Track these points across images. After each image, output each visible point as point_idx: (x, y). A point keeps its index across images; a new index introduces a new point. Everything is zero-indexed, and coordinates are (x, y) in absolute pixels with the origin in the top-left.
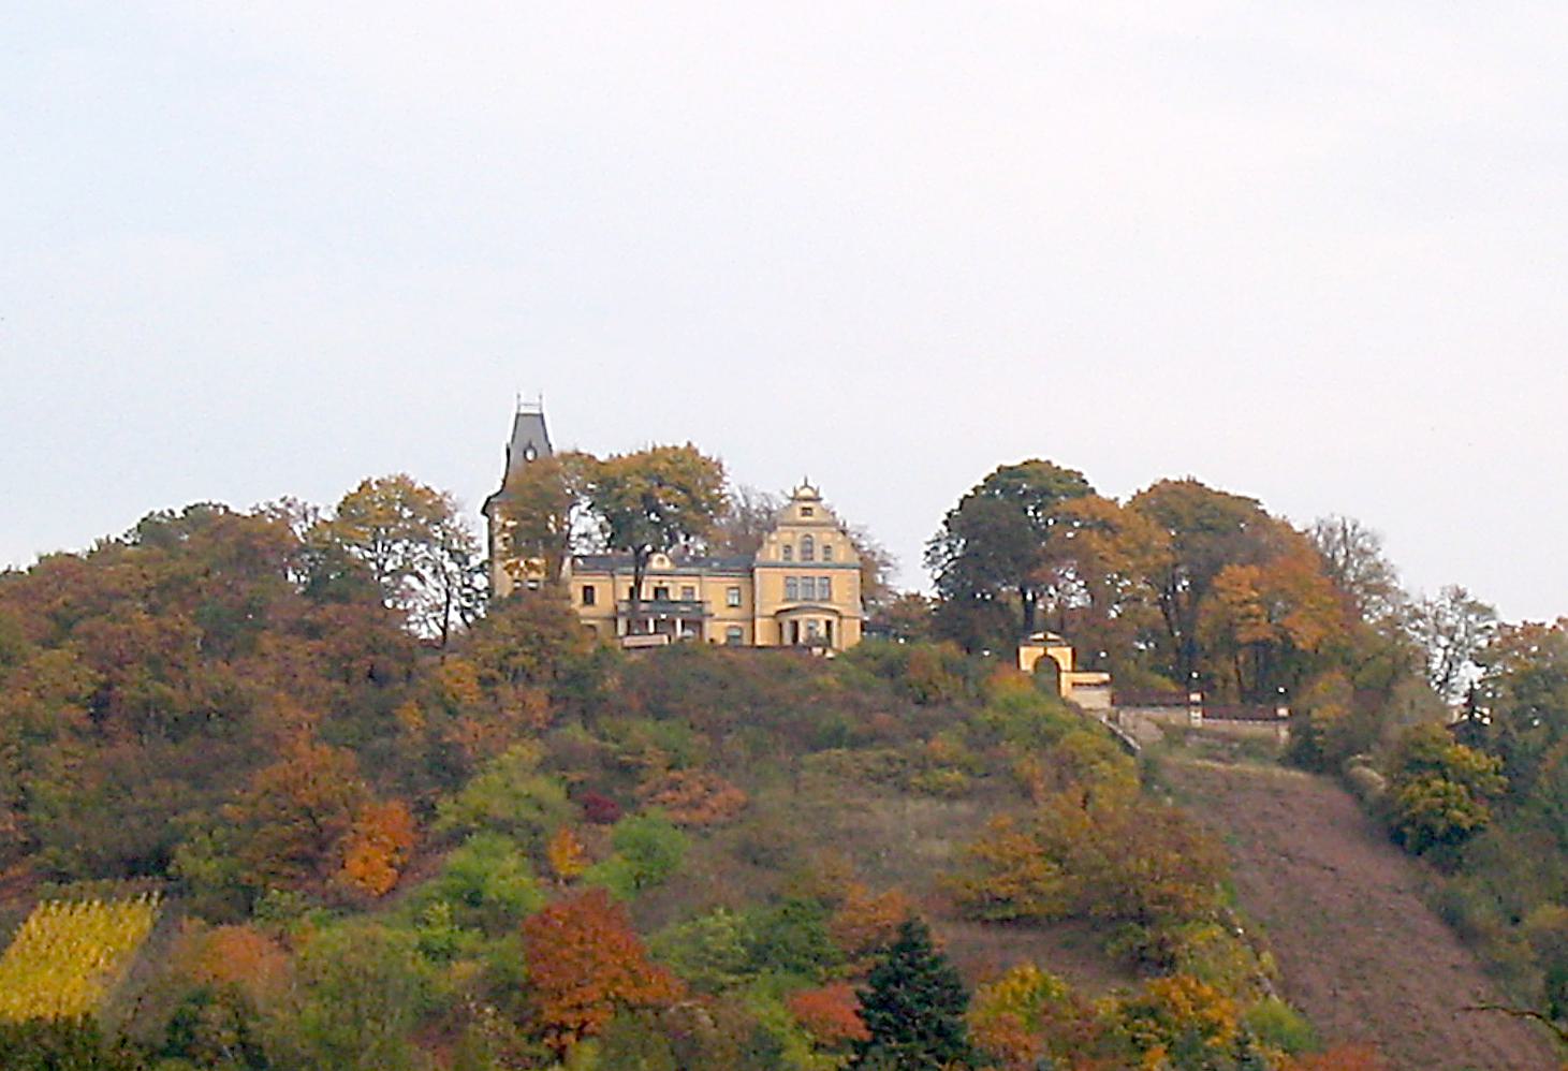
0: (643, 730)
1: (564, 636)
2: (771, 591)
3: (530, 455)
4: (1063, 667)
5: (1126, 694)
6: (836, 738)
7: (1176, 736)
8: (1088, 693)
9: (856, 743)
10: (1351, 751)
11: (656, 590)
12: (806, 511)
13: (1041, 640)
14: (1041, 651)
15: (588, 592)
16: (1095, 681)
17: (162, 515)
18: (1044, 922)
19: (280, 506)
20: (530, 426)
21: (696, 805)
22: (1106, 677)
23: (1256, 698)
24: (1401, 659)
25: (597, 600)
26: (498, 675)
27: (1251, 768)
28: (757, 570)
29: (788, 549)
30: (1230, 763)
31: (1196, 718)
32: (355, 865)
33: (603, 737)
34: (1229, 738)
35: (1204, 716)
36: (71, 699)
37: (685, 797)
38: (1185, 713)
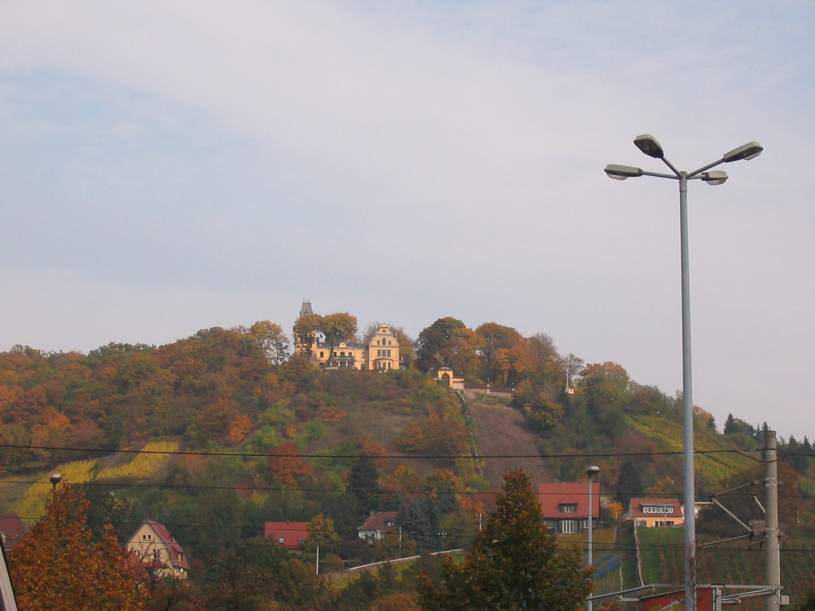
0: (321, 395)
1: (304, 368)
2: (373, 354)
3: (306, 315)
5: (468, 385)
6: (377, 398)
7: (480, 397)
8: (456, 385)
9: (383, 399)
10: (525, 402)
11: (341, 353)
14: (444, 372)
15: (322, 354)
17: (204, 330)
19: (238, 328)
20: (307, 305)
21: (332, 417)
22: (463, 380)
23: (508, 386)
24: (557, 373)
25: (324, 356)
26: (284, 378)
27: (497, 407)
28: (370, 348)
29: (378, 342)
30: (492, 405)
31: (488, 392)
32: (232, 433)
33: (310, 397)
34: (495, 397)
35: (491, 391)
36: (169, 383)
37: (329, 414)
38: (485, 390)
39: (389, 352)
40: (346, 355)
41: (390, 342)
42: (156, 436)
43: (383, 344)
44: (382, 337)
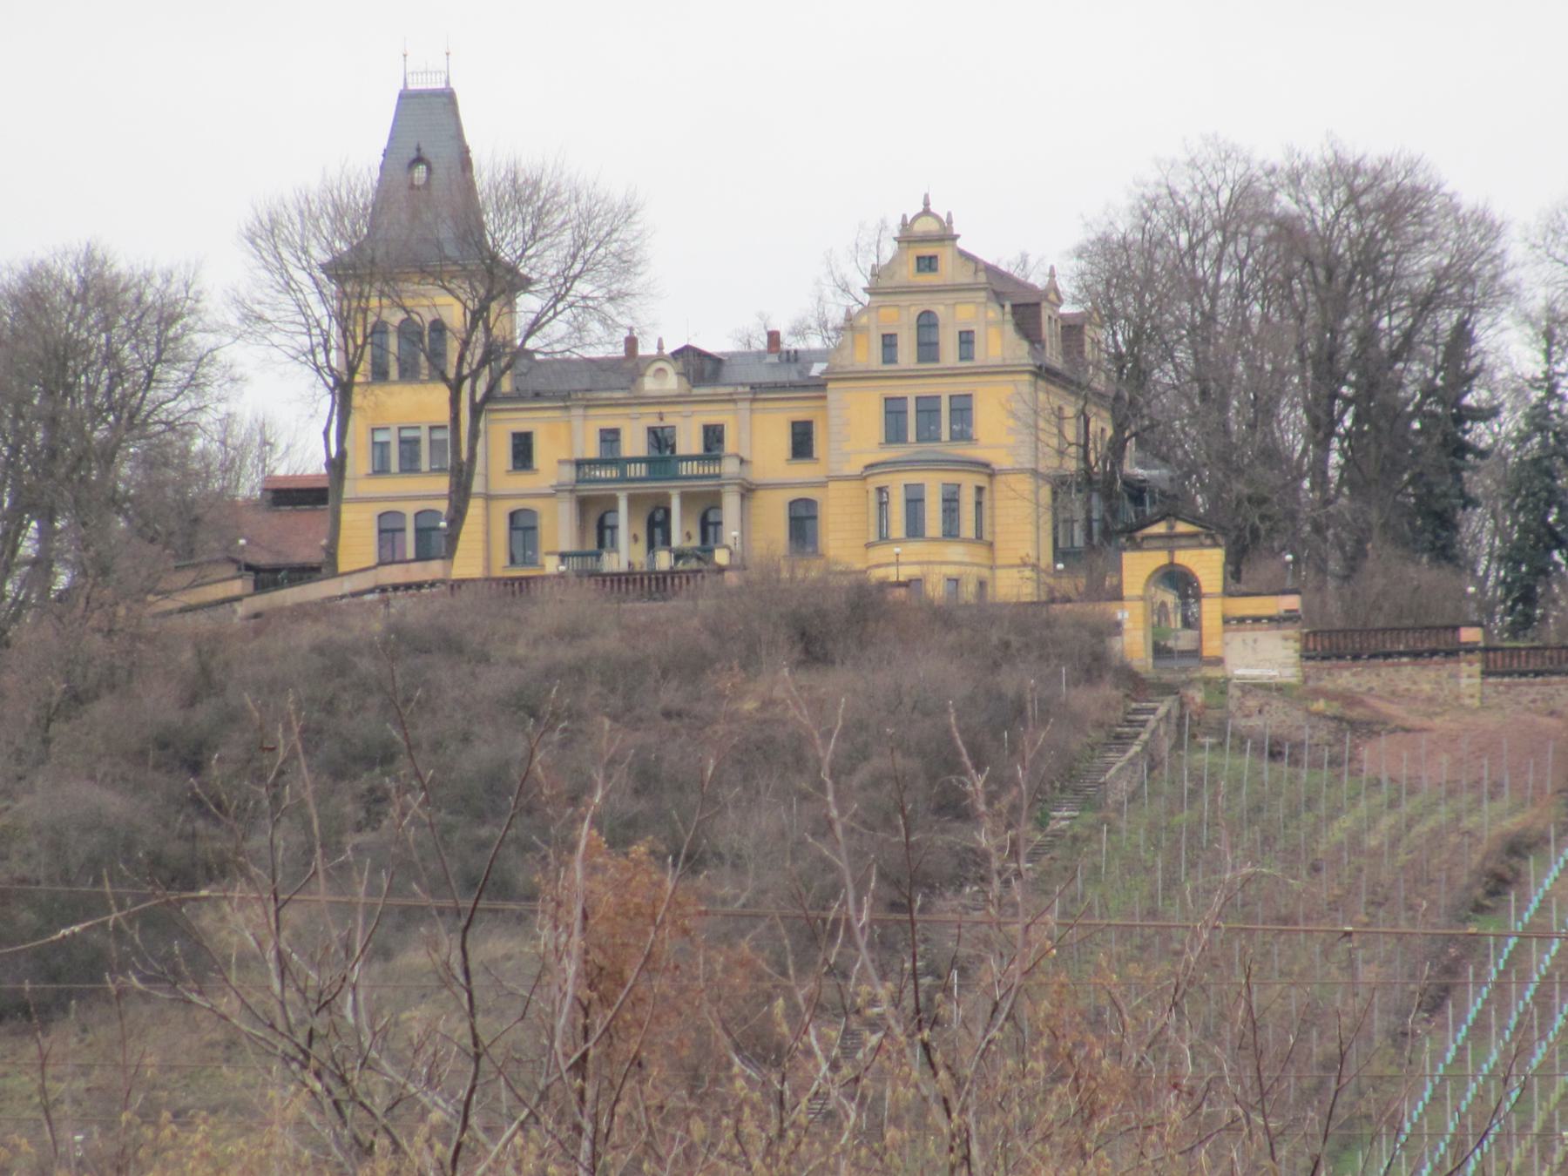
4: (1206, 587)
12: (927, 264)
13: (1159, 536)
16: (1273, 612)
18: (1446, 980)
22: (1292, 602)
29: (889, 342)
39: (962, 408)
40: (681, 450)
41: (966, 339)
42: (892, 261)
43: (921, 359)
44: (912, 308)
